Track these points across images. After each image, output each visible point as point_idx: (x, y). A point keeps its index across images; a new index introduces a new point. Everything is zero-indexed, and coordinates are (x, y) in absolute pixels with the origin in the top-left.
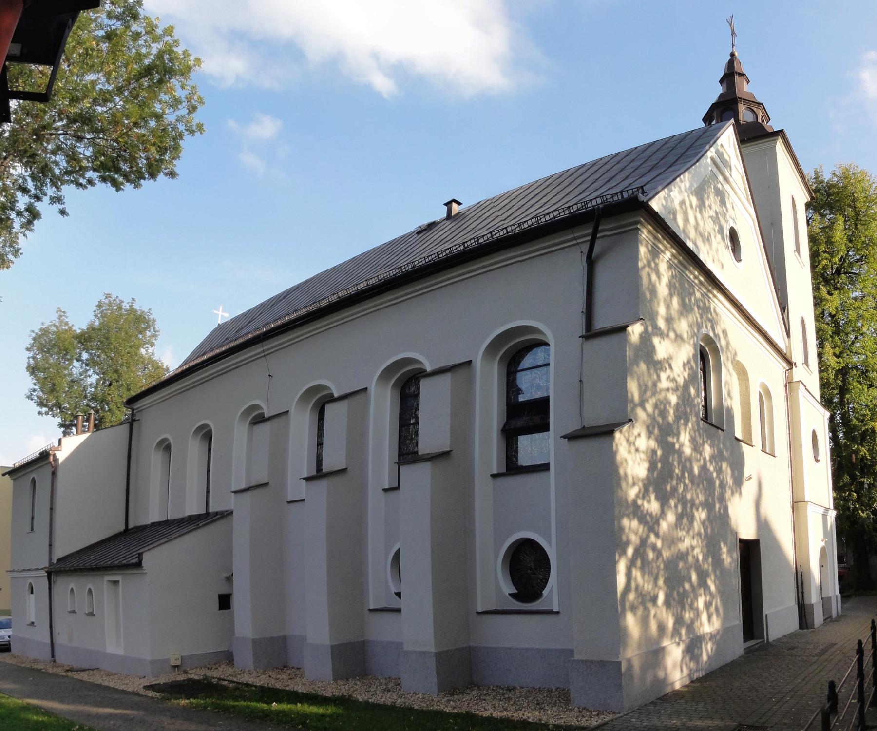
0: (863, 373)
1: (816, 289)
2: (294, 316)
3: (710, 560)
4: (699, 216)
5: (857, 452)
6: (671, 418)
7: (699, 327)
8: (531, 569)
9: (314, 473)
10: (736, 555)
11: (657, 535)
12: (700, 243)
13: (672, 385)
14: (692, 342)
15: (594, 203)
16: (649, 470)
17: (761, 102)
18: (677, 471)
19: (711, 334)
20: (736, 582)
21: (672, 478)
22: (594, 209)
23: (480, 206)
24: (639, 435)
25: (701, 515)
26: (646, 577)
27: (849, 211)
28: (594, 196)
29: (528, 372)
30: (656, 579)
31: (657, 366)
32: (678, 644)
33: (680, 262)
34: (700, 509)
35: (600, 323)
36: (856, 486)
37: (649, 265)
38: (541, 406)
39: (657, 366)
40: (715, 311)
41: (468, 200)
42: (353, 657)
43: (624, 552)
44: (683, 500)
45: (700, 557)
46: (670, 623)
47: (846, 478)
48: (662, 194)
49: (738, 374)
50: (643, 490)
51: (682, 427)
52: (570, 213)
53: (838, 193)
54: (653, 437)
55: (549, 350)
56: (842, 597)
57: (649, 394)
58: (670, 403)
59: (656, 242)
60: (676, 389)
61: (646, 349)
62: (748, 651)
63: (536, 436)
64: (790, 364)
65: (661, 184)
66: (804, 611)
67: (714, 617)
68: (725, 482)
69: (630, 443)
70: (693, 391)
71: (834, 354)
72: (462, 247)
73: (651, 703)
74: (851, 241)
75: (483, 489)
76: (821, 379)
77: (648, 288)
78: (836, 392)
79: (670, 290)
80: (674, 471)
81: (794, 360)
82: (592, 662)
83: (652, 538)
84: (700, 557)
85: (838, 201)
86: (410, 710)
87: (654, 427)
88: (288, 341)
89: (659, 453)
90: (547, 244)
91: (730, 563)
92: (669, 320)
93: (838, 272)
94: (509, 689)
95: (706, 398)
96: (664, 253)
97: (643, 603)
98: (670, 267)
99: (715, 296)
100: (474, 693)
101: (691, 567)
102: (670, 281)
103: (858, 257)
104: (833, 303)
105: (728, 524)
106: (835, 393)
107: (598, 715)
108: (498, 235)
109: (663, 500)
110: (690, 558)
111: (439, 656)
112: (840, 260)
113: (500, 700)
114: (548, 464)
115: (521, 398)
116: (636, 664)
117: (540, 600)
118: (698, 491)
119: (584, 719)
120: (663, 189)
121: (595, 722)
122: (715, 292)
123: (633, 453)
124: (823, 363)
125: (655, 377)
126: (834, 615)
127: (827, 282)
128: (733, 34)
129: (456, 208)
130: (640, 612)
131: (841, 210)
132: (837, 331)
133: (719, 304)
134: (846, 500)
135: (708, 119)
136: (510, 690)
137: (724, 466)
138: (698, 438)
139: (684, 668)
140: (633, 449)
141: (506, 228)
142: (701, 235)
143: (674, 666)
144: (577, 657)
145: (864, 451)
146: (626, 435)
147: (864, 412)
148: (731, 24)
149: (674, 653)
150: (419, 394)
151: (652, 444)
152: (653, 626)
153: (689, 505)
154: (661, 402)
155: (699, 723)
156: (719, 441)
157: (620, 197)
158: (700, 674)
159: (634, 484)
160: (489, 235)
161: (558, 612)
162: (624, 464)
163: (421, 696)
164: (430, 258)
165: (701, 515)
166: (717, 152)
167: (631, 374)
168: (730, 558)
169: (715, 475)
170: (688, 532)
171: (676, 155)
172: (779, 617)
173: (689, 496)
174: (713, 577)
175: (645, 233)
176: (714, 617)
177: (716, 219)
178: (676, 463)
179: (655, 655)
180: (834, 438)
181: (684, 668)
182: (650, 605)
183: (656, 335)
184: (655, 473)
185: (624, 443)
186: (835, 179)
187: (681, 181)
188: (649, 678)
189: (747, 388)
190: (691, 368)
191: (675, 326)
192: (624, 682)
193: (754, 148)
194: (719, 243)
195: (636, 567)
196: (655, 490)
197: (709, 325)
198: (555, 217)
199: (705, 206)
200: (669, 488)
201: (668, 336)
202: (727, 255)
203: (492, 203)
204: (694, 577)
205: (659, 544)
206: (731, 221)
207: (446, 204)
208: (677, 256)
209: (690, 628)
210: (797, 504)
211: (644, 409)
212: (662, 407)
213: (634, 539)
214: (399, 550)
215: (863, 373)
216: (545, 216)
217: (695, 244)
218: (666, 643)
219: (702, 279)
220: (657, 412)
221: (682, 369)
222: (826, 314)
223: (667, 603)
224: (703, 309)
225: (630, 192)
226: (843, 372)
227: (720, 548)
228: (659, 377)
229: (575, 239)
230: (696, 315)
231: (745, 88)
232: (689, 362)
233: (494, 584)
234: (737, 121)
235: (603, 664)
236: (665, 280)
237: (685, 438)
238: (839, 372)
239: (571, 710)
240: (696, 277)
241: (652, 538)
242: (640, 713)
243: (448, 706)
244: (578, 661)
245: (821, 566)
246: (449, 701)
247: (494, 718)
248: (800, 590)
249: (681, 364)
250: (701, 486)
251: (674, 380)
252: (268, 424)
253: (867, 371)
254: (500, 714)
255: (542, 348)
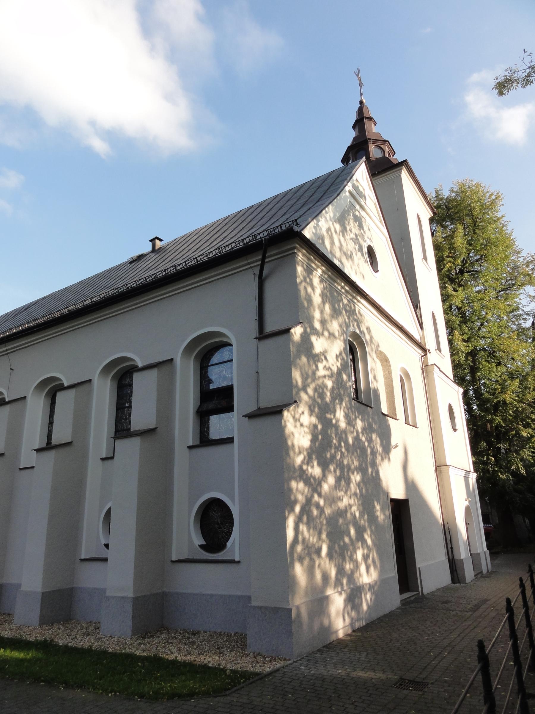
0: (490, 354)
1: (443, 287)
2: (33, 324)
3: (366, 516)
4: (342, 239)
5: (491, 421)
6: (328, 399)
7: (348, 326)
8: (218, 524)
9: (44, 445)
10: (389, 512)
11: (320, 495)
12: (344, 260)
13: (328, 373)
14: (342, 338)
15: (262, 235)
16: (312, 441)
17: (386, 139)
18: (335, 441)
19: (358, 331)
20: (389, 536)
21: (331, 447)
22: (262, 240)
23: (176, 242)
24: (303, 413)
25: (356, 478)
26: (311, 531)
27: (468, 220)
28: (261, 230)
29: (217, 367)
30: (320, 533)
31: (315, 358)
32: (341, 593)
33: (329, 276)
34: (355, 473)
35: (269, 328)
36: (493, 450)
37: (305, 280)
38: (228, 391)
39: (315, 358)
40: (359, 312)
41: (168, 238)
42: (61, 604)
43: (292, 510)
44: (340, 466)
45: (357, 514)
46: (333, 573)
47: (484, 444)
48: (312, 224)
49: (382, 362)
50: (307, 458)
51: (338, 406)
52: (244, 244)
53: (457, 206)
54: (314, 414)
55: (232, 349)
56: (491, 554)
57: (309, 380)
58: (327, 387)
59: (310, 263)
60: (331, 376)
61: (306, 345)
62: (405, 603)
63: (223, 415)
64: (425, 351)
65: (310, 217)
66: (454, 566)
67: (372, 569)
68: (375, 450)
69: (296, 420)
70: (345, 377)
71: (463, 340)
72: (164, 273)
73: (319, 650)
74: (470, 245)
75: (181, 458)
76: (453, 361)
77: (305, 299)
78: (467, 371)
79: (322, 298)
80: (332, 441)
81: (427, 347)
82: (266, 608)
83: (316, 497)
84: (357, 514)
85: (458, 212)
86: (105, 653)
87: (314, 407)
88: (26, 343)
89: (320, 427)
90: (227, 269)
91: (384, 520)
92: (323, 322)
93: (461, 272)
94: (194, 634)
95: (356, 382)
96: (317, 271)
97: (309, 554)
98: (322, 281)
99: (359, 301)
100: (163, 636)
101: (350, 523)
102: (322, 292)
103: (478, 257)
104: (458, 297)
105: (380, 485)
106: (466, 372)
107: (271, 661)
108: (190, 264)
109: (324, 466)
110: (349, 515)
111: (136, 600)
112: (462, 262)
113: (185, 644)
114: (233, 438)
115: (212, 387)
116: (304, 611)
117: (225, 551)
118: (353, 457)
119: (258, 665)
120: (312, 220)
121: (268, 669)
122: (359, 298)
123: (298, 428)
124: (454, 349)
125: (314, 367)
126: (485, 571)
127: (452, 281)
128: (361, 84)
129: (158, 244)
130: (306, 562)
131: (460, 220)
132: (464, 320)
133: (362, 307)
134: (485, 463)
135: (345, 160)
136: (195, 635)
137: (374, 436)
138: (351, 414)
139: (346, 617)
140: (298, 424)
141: (196, 258)
142: (345, 254)
143: (338, 613)
144: (254, 603)
145: (498, 419)
146: (293, 413)
147: (494, 386)
148: (358, 76)
149: (337, 601)
150: (132, 384)
151: (314, 420)
152: (318, 576)
153: (346, 470)
154: (320, 387)
155: (361, 674)
156: (368, 416)
157: (280, 229)
158: (362, 623)
159: (300, 453)
160: (184, 264)
161: (239, 562)
162: (291, 436)
163: (116, 639)
164: (140, 282)
165: (356, 478)
166: (354, 186)
167: (295, 366)
168: (383, 515)
169: (366, 444)
170: (346, 492)
171: (323, 191)
172: (433, 574)
173: (345, 462)
174: (369, 533)
175: (301, 256)
176: (372, 569)
177: (356, 240)
178: (333, 435)
179: (320, 603)
180: (469, 411)
181: (346, 617)
182: (315, 557)
183: (314, 334)
184: (317, 444)
185: (291, 420)
186: (454, 194)
187: (326, 213)
188: (316, 626)
189: (390, 372)
190: (343, 359)
191: (328, 326)
192: (294, 628)
193: (383, 179)
194: (359, 259)
195: (302, 522)
196: (317, 458)
197: (355, 324)
198: (233, 248)
199: (346, 231)
200: (328, 455)
201: (323, 334)
202: (367, 268)
203: (185, 239)
204: (353, 532)
205: (322, 502)
206: (368, 241)
207: (151, 241)
208: (327, 272)
209: (351, 578)
210: (440, 468)
211: (306, 393)
212: (321, 391)
213: (301, 498)
214: (110, 508)
215: (490, 354)
216: (225, 247)
217: (340, 261)
218: (330, 592)
219: (347, 288)
220: (316, 395)
221: (335, 360)
222: (454, 308)
223: (330, 555)
224: (349, 312)
225: (287, 225)
226: (473, 354)
227: (374, 507)
228: (317, 367)
229: (249, 264)
230: (344, 317)
231: (373, 130)
232: (341, 354)
233: (187, 536)
234: (368, 158)
235: (276, 610)
236: (318, 291)
237: (340, 414)
238: (468, 354)
239: (247, 655)
240: (342, 287)
241: (316, 497)
242: (309, 660)
243: (139, 650)
244: (255, 607)
245: (467, 524)
246: (140, 644)
247: (178, 662)
248: (449, 546)
249: (335, 356)
250: (355, 454)
251: (329, 369)
252: (7, 408)
253: (494, 352)
254: (184, 658)
255: (227, 348)
